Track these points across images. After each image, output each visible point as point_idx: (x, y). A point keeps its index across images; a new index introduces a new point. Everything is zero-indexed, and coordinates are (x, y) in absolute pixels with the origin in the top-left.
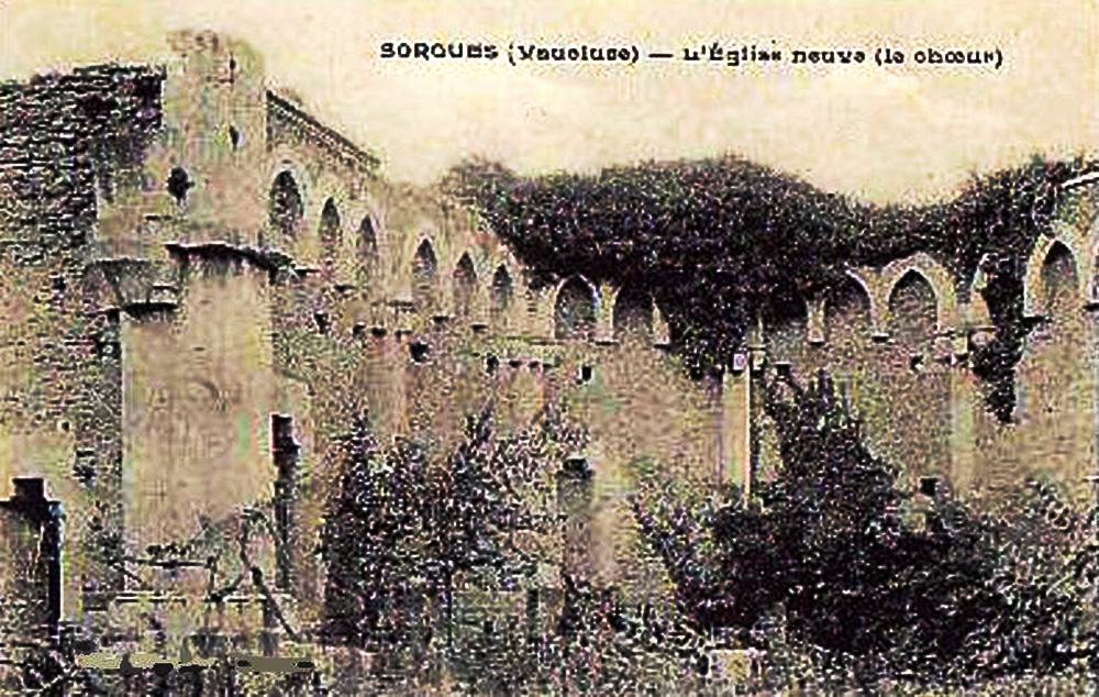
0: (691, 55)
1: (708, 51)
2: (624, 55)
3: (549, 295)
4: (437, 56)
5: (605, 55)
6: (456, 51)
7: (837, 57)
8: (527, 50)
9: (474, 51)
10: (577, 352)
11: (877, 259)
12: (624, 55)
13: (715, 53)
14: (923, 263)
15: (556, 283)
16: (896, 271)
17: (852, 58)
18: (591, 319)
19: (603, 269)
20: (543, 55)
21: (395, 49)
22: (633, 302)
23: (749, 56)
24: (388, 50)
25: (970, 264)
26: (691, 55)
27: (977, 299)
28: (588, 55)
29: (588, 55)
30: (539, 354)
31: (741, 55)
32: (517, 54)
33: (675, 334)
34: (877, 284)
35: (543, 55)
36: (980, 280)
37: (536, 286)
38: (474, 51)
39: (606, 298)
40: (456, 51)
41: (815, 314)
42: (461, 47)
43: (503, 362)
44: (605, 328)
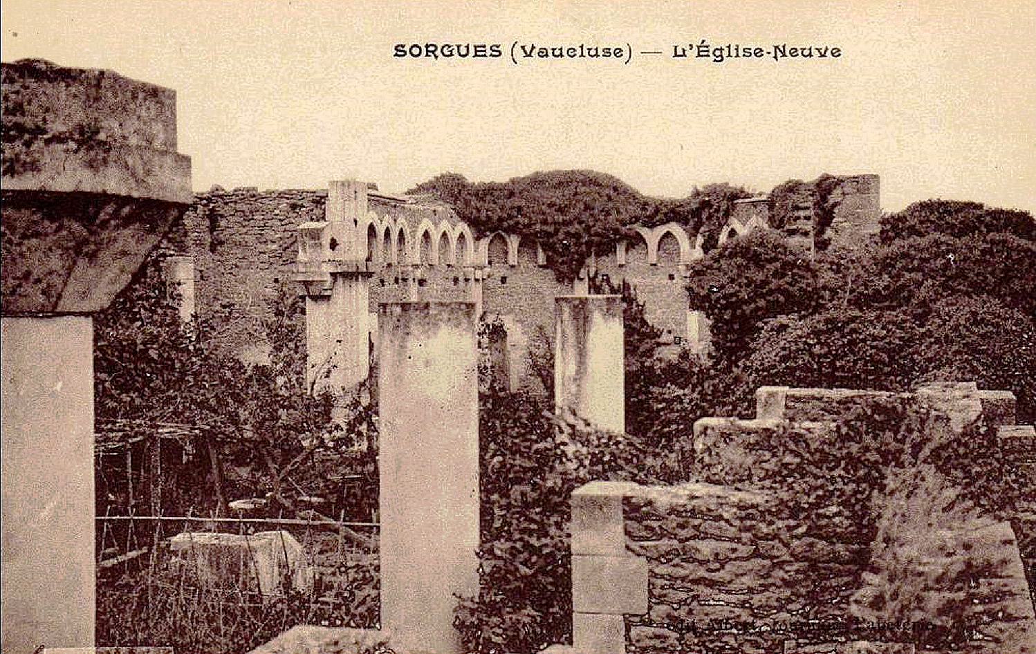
0: (680, 52)
1: (695, 48)
2: (618, 52)
3: (484, 243)
4: (412, 55)
5: (564, 53)
6: (463, 51)
7: (815, 52)
8: (528, 49)
9: (479, 51)
10: (499, 271)
11: (651, 224)
12: (618, 52)
13: (703, 50)
14: (675, 228)
15: (488, 236)
16: (661, 230)
17: (828, 53)
18: (506, 253)
19: (512, 230)
20: (543, 53)
21: (612, 51)
22: (527, 243)
23: (733, 53)
24: (400, 51)
25: (696, 229)
26: (680, 52)
27: (698, 248)
28: (586, 53)
29: (586, 53)
30: (479, 274)
31: (725, 53)
32: (519, 53)
33: (548, 259)
34: (652, 236)
35: (543, 53)
36: (700, 240)
37: (478, 239)
38: (479, 51)
39: (513, 242)
40: (463, 51)
41: (621, 249)
42: (467, 47)
43: (461, 279)
44: (513, 258)
